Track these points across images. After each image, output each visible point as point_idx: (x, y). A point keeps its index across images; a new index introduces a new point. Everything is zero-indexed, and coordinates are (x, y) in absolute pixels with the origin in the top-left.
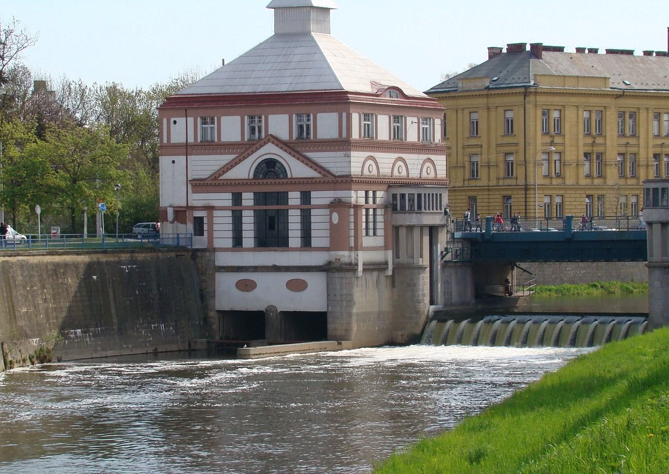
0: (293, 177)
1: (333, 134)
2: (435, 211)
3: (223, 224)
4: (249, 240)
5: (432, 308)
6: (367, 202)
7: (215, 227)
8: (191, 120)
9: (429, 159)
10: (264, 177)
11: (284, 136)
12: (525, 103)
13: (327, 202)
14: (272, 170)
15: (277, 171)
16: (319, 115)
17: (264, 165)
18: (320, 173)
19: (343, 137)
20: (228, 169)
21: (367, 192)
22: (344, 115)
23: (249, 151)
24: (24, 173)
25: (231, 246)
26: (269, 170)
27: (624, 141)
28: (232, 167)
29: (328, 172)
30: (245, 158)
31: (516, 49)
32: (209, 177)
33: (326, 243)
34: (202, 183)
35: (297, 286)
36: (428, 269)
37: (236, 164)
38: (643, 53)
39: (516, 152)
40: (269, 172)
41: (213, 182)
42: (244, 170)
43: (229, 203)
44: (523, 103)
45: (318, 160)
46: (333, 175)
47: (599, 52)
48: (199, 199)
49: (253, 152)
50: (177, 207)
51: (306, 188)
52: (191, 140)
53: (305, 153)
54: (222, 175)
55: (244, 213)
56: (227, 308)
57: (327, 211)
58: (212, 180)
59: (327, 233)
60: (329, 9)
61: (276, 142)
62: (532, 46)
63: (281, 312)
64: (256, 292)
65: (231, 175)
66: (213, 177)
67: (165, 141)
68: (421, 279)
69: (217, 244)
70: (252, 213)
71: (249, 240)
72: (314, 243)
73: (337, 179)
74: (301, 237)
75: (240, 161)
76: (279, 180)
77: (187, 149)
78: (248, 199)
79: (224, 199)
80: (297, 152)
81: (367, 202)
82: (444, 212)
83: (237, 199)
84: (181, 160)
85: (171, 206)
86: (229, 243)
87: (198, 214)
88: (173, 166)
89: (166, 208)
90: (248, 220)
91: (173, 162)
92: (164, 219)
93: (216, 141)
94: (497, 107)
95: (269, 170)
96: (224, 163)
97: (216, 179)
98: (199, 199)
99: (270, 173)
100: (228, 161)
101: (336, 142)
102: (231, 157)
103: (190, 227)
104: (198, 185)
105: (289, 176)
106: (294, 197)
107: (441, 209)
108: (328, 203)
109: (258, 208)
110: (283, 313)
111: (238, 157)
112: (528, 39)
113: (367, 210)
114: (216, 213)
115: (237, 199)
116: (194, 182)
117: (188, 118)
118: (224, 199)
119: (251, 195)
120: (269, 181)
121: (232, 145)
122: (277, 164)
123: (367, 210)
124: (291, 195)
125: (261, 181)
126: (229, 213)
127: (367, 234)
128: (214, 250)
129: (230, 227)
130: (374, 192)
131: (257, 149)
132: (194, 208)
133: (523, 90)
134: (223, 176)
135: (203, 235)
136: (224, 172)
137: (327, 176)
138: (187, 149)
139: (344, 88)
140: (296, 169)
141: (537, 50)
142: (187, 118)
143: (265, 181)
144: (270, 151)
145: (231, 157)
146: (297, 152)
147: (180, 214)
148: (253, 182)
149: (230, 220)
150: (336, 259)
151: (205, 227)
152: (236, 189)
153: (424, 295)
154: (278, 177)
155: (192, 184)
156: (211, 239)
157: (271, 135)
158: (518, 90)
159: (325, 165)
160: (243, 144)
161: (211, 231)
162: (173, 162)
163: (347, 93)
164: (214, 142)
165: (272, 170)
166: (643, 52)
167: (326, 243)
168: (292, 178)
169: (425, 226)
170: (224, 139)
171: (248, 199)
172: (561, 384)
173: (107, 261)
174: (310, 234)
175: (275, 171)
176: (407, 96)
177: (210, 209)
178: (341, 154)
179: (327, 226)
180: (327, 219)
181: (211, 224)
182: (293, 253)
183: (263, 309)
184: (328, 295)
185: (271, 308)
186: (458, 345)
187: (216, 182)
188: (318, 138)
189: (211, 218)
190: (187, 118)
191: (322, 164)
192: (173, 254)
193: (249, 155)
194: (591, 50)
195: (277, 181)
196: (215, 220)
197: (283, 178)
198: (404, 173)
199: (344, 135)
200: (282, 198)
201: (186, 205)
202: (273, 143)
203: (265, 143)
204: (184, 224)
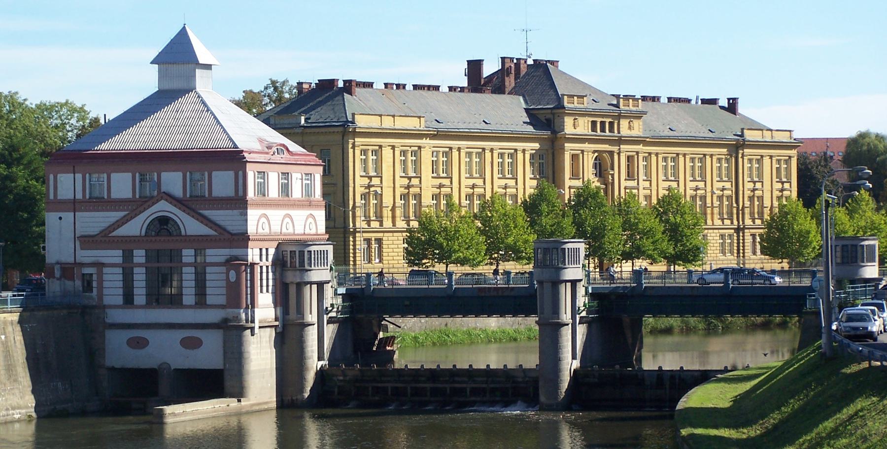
0: (188, 234)
1: (230, 192)
2: (320, 268)
3: (113, 280)
4: (140, 297)
5: (321, 363)
6: (261, 260)
7: (105, 284)
8: (79, 176)
9: (311, 214)
10: (157, 235)
11: (178, 192)
12: (343, 142)
13: (222, 259)
14: (165, 227)
15: (170, 228)
16: (214, 173)
17: (157, 222)
18: (216, 231)
19: (240, 195)
20: (119, 227)
21: (261, 249)
22: (241, 173)
23: (142, 208)
24: (405, 325)
25: (121, 303)
26: (162, 227)
27: (437, 182)
28: (123, 224)
29: (225, 230)
30: (136, 215)
31: (326, 85)
32: (98, 234)
33: (222, 300)
34: (91, 239)
35: (192, 344)
36: (316, 326)
37: (127, 221)
38: (448, 89)
39: (334, 193)
40: (162, 229)
41: (103, 239)
42: (135, 227)
43: (119, 260)
44: (341, 143)
45: (213, 218)
46: (228, 232)
47: (407, 87)
48: (87, 256)
49: (145, 210)
50: (64, 264)
51: (200, 243)
52: (79, 196)
53: (201, 211)
54: (113, 231)
55: (136, 270)
56: (117, 366)
57: (223, 269)
58: (102, 237)
59: (224, 291)
60: (211, 65)
61: (168, 198)
62: (345, 82)
63: (175, 369)
64: (148, 349)
65: (123, 231)
66: (103, 234)
67: (52, 197)
68: (310, 335)
69: (107, 300)
70: (143, 270)
71: (140, 297)
72: (210, 300)
73: (234, 237)
74: (196, 295)
75: (132, 218)
76: (173, 238)
77: (74, 205)
78: (139, 255)
79: (114, 256)
80: (194, 210)
81: (261, 260)
82: (329, 268)
83: (128, 256)
84: (68, 216)
85: (58, 263)
86: (120, 300)
87: (87, 271)
88: (60, 222)
89: (52, 264)
90: (140, 277)
91: (60, 218)
92: (50, 275)
93: (106, 197)
94: (313, 146)
95: (162, 227)
96: (114, 220)
97: (105, 236)
98: (87, 256)
99: (163, 231)
100: (117, 219)
101: (232, 200)
102: (122, 214)
103: (78, 283)
104: (87, 241)
105: (183, 233)
106: (188, 255)
107: (327, 265)
108: (224, 261)
109: (149, 265)
110: (176, 370)
111: (128, 214)
112: (340, 76)
113: (261, 267)
114: (106, 270)
115: (128, 256)
116: (81, 239)
117: (76, 175)
118: (114, 256)
119: (142, 252)
120: (163, 239)
121: (122, 202)
122: (171, 222)
123: (261, 267)
124: (185, 252)
125: (153, 239)
126: (120, 270)
127: (261, 292)
128: (105, 307)
129: (121, 284)
130: (267, 249)
131: (149, 207)
132: (82, 265)
133: (340, 129)
134: (114, 233)
135: (92, 291)
136: (114, 230)
137: (223, 234)
138: (74, 205)
139: (239, 147)
140: (191, 226)
141: (349, 87)
142: (74, 174)
143: (158, 238)
144: (163, 208)
145: (122, 214)
146: (194, 210)
147: (68, 270)
148: (145, 239)
149: (121, 277)
150: (234, 317)
151: (95, 284)
152: (127, 245)
153: (312, 351)
154: (170, 234)
155: (80, 241)
156: (101, 296)
157: (164, 192)
158: (336, 129)
159: (222, 223)
160: (134, 201)
161: (101, 287)
162: (60, 218)
163: (242, 151)
164: (104, 198)
165: (165, 227)
166: (449, 87)
167: (222, 300)
168: (186, 236)
169: (314, 283)
170: (114, 195)
171: (139, 255)
172: (5, 370)
173: (12, 321)
174: (205, 291)
175: (169, 229)
176: (291, 152)
177: (100, 265)
178: (236, 212)
179: (224, 284)
180: (224, 276)
181: (101, 281)
182: (188, 310)
183: (156, 367)
184: (225, 353)
185: (165, 366)
186: (246, 386)
187: (105, 238)
188: (213, 196)
189: (100, 274)
190: (74, 174)
191: (218, 222)
192: (65, 312)
193: (141, 212)
194: (398, 86)
195: (170, 238)
196: (105, 277)
197: (177, 236)
198: (291, 231)
199: (241, 193)
200: (175, 256)
201: (73, 262)
202: (166, 200)
203: (158, 201)
204: (71, 280)
